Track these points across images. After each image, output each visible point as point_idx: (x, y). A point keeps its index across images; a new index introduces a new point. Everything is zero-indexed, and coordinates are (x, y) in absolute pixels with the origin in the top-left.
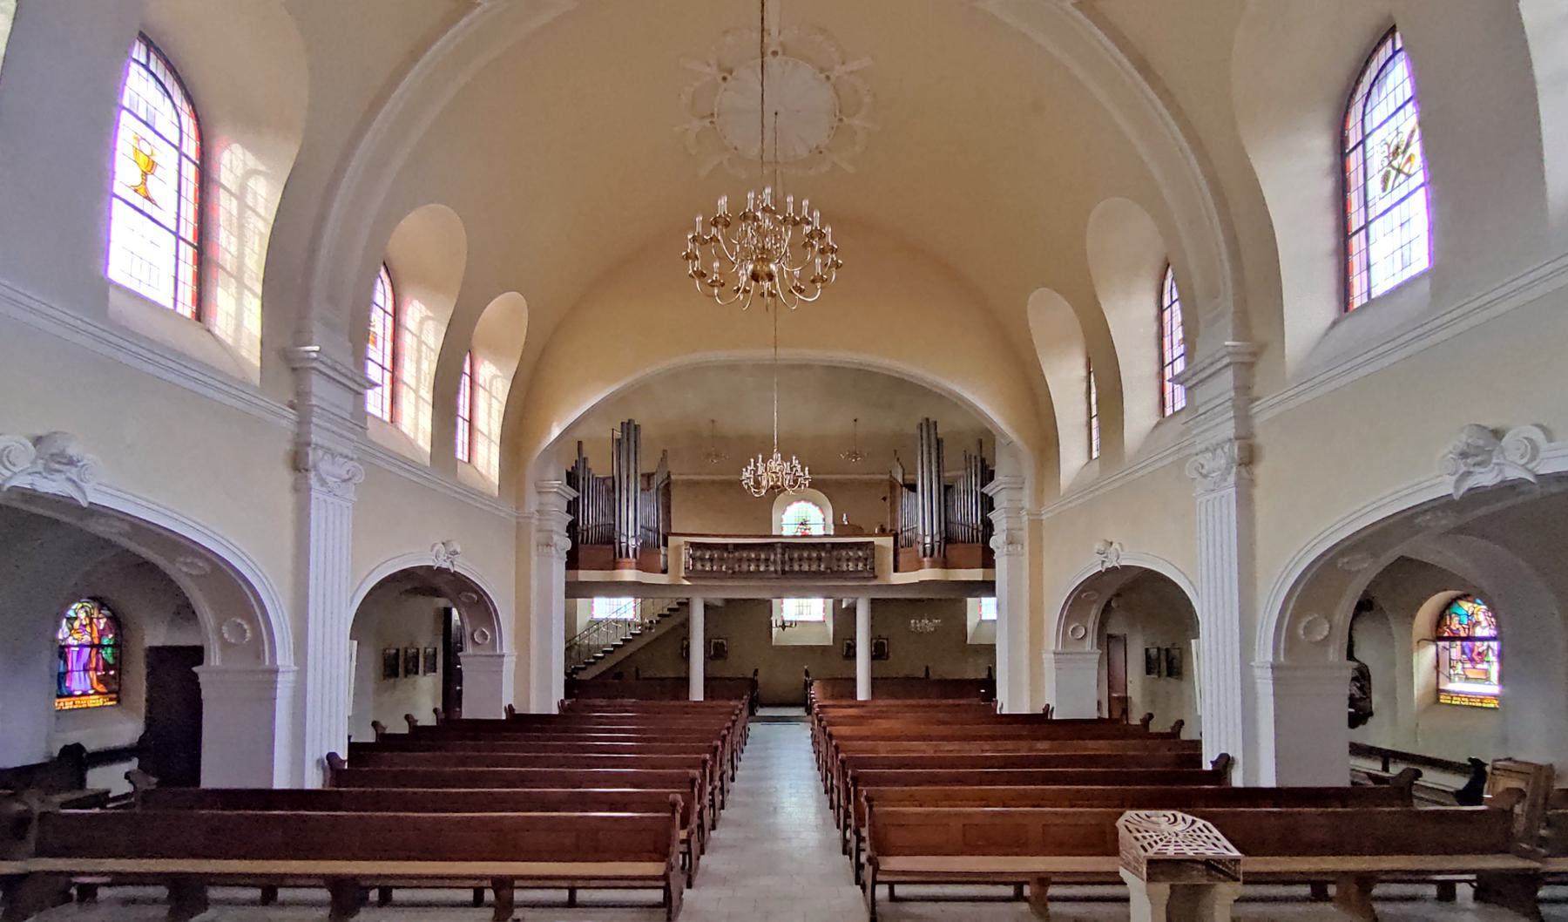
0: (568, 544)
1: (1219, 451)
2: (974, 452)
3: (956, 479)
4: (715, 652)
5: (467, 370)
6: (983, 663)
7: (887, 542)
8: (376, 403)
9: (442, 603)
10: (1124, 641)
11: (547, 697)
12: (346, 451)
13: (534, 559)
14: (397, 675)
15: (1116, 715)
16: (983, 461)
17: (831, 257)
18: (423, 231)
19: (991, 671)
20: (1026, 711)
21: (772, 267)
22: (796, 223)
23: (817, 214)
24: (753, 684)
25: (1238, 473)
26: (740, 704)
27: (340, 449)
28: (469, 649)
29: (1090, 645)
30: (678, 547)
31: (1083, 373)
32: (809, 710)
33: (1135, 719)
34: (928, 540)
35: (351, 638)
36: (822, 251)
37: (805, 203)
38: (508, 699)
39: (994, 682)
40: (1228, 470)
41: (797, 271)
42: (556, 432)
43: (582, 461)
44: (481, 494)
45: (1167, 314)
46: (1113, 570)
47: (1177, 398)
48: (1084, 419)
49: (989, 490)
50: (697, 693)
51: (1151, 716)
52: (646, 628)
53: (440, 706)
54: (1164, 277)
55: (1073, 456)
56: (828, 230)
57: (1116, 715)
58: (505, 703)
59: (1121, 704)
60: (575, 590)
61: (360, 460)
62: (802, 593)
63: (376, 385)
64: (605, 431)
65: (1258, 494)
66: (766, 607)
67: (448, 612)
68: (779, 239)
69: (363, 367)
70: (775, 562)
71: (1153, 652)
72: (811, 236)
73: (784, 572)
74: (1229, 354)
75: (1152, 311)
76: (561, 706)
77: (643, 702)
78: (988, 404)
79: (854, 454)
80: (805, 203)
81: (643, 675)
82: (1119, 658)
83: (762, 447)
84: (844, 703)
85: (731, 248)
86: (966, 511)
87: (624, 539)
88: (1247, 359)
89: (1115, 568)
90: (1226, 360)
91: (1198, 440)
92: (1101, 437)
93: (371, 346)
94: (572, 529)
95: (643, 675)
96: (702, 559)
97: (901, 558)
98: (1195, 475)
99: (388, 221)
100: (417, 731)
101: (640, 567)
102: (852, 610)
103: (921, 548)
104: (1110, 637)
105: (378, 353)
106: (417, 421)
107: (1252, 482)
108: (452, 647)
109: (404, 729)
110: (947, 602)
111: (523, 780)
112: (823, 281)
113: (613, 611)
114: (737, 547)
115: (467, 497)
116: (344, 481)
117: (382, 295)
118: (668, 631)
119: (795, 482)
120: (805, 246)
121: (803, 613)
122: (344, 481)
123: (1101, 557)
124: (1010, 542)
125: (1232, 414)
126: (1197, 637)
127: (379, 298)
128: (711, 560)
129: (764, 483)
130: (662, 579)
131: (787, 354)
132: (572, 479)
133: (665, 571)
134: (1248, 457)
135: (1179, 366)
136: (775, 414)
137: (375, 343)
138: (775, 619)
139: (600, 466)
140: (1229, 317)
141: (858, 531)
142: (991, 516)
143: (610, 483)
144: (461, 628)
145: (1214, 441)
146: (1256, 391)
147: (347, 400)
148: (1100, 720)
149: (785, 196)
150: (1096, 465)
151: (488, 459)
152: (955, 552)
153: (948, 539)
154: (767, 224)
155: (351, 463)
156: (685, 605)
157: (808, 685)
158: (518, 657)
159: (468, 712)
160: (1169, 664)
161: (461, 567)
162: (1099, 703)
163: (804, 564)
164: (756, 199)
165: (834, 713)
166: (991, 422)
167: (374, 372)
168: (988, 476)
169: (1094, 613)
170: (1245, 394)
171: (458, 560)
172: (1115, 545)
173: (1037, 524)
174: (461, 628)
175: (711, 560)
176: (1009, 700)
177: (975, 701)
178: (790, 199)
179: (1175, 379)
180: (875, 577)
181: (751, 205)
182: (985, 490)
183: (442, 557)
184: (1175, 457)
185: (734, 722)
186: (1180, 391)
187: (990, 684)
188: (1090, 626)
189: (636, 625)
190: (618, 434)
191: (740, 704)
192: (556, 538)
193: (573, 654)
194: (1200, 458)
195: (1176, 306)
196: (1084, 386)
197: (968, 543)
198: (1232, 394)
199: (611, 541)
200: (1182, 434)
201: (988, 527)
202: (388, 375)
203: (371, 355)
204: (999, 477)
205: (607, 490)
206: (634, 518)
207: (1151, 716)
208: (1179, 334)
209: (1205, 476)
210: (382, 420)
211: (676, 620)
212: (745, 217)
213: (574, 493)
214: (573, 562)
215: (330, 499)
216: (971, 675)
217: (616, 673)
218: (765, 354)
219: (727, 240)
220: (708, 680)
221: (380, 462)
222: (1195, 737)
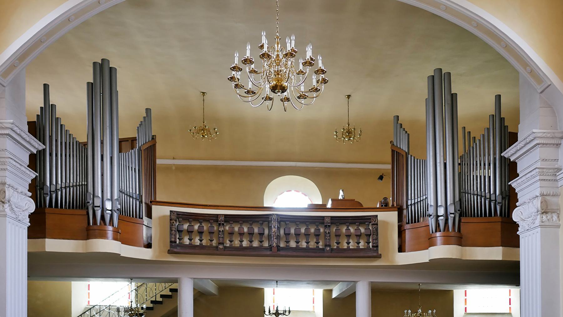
0: (31, 207)
7: (391, 217)
34: (441, 211)
49: (510, 153)
62: (292, 277)
87: (98, 202)
94: (36, 188)
97: (408, 235)
101: (119, 236)
103: (432, 222)
111: (466, 207)
114: (229, 219)
133: (149, 246)
141: (358, 206)
142: (514, 184)
153: (463, 212)
180: (379, 257)
182: (506, 154)
199: (83, 205)
201: (510, 198)
206: (112, 183)
211: (166, 308)
214: (38, 227)
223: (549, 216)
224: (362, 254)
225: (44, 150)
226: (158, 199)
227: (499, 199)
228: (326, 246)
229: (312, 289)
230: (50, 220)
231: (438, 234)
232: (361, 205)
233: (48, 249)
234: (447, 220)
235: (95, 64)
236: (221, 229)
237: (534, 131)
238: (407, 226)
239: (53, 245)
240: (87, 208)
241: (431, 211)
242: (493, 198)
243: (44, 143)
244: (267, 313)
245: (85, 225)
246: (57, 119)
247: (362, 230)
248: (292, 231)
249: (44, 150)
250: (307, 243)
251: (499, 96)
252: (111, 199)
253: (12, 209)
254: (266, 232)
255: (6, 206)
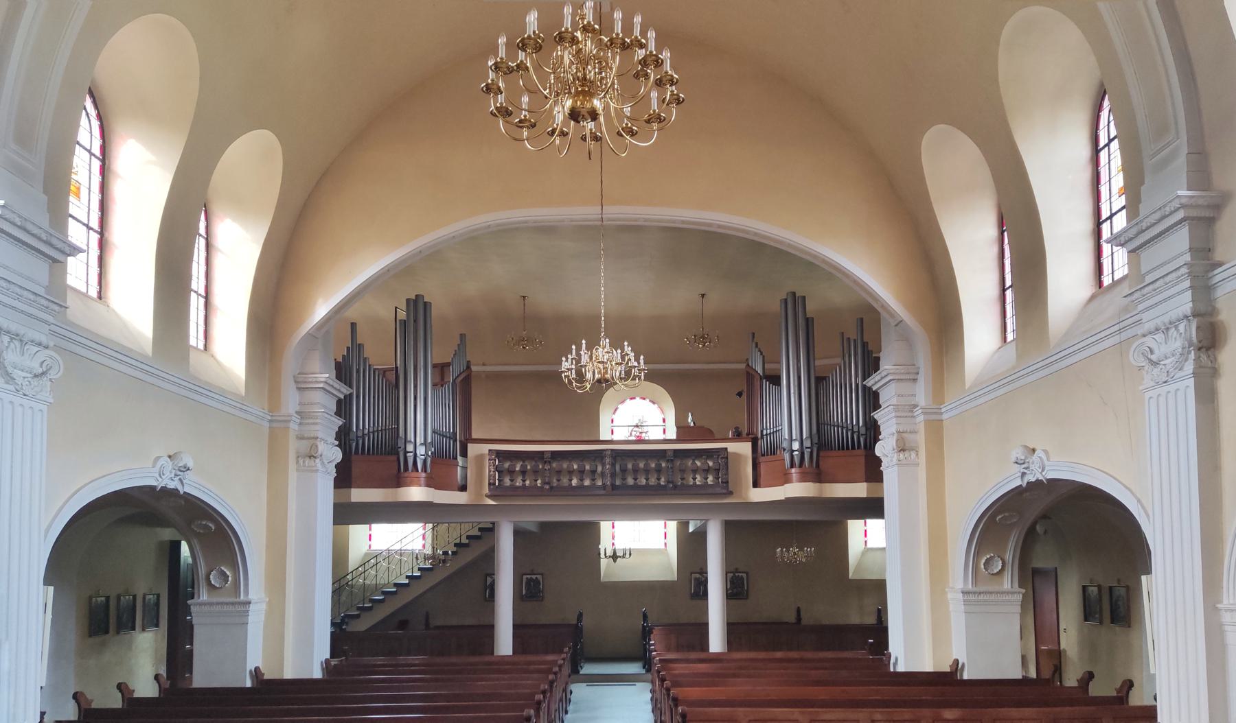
0: (338, 455)
1: (1172, 331)
2: (852, 334)
3: (833, 367)
4: (528, 592)
5: (202, 231)
6: (870, 604)
8: (79, 273)
9: (167, 534)
10: (1052, 576)
11: (305, 653)
12: (38, 337)
13: (293, 476)
14: (107, 632)
15: (1046, 674)
16: (865, 345)
17: (670, 90)
18: (142, 52)
19: (881, 615)
20: (929, 668)
21: (597, 103)
22: (625, 47)
23: (652, 34)
24: (576, 631)
25: (1197, 359)
26: (560, 659)
27: (31, 334)
28: (204, 596)
29: (1008, 582)
30: (480, 458)
31: (991, 231)
32: (648, 665)
33: (1071, 679)
34: (796, 446)
35: (47, 581)
36: (659, 83)
37: (637, 20)
38: (255, 658)
39: (885, 630)
40: (1184, 356)
41: (627, 110)
42: (321, 310)
43: (356, 348)
44: (223, 393)
45: (1103, 155)
46: (1053, 482)
47: (1117, 262)
48: (994, 291)
49: (873, 382)
50: (505, 644)
51: (1090, 676)
52: (437, 561)
53: (163, 671)
54: (1099, 108)
55: (982, 336)
56: (666, 55)
57: (1046, 674)
58: (251, 666)
59: (1052, 659)
60: (346, 514)
61: (57, 348)
63: (81, 251)
64: (385, 310)
65: (1225, 387)
66: (590, 532)
67: (176, 546)
68: (603, 65)
69: (63, 228)
70: (603, 475)
71: (1093, 590)
72: (644, 62)
73: (614, 487)
74: (1183, 206)
75: (1085, 151)
76: (326, 666)
77: (439, 660)
78: (866, 267)
79: (704, 338)
80: (637, 20)
81: (435, 622)
82: (1049, 599)
83: (583, 329)
84: (693, 655)
85: (544, 78)
86: (845, 410)
87: (410, 448)
88: (1207, 213)
89: (1039, 482)
90: (1180, 215)
91: (1145, 316)
92: (1017, 314)
93: (72, 199)
94: (343, 437)
95: (435, 622)
96: (511, 472)
97: (763, 468)
98: (1142, 362)
99: (98, 31)
100: (134, 705)
101: (432, 483)
102: (701, 535)
103: (787, 457)
104: (1036, 572)
105: (82, 206)
106: (132, 304)
107: (1215, 372)
108: (180, 589)
109: (116, 702)
110: (823, 526)
112: (660, 120)
113: (402, 540)
115: (200, 396)
116: (35, 376)
117: (87, 132)
118: (462, 568)
119: (628, 373)
120: (637, 76)
121: (640, 542)
122: (35, 376)
123: (1020, 469)
124: (902, 448)
125: (1187, 283)
126: (1148, 571)
127: (83, 136)
128: (523, 472)
129: (589, 376)
130: (459, 498)
131: (617, 212)
132: (343, 371)
133: (463, 488)
134: (1209, 338)
135: (1120, 222)
136: (603, 288)
137: (78, 195)
138: (605, 545)
139: (380, 353)
140: (1181, 162)
141: (708, 435)
142: (877, 415)
143: (392, 376)
144: (194, 567)
145: (1166, 319)
146: (1218, 256)
147: (40, 270)
148: (1025, 681)
149: (612, 10)
150: (1011, 350)
151: (227, 346)
152: (831, 461)
154: (589, 46)
155: (47, 352)
156: (489, 531)
157: (646, 633)
158: (269, 603)
159: (202, 677)
160: (1115, 608)
161: (193, 486)
162: (1024, 658)
163: (640, 478)
164: (574, 15)
165: (680, 669)
166: (876, 298)
167: (76, 234)
168: (871, 364)
169: (1010, 553)
170: (1204, 261)
171: (189, 477)
172: (1039, 453)
173: (935, 428)
174: (194, 567)
175: (523, 472)
176: (910, 651)
177: (861, 654)
178: (618, 15)
179: (1116, 240)
180: (731, 493)
181: (567, 23)
183: (168, 474)
184: (1116, 339)
185: (552, 683)
186: (1121, 255)
187: (879, 632)
188: (1009, 556)
189: (426, 558)
190: (402, 315)
191: (560, 659)
192: (322, 447)
193: (343, 598)
194: (1149, 341)
195: (1115, 145)
196: (995, 250)
197: (848, 449)
198: (1187, 257)
200: (1126, 309)
201: (873, 431)
202: (95, 237)
203: (72, 210)
204: (886, 366)
205: (389, 383)
206: (421, 424)
207: (1090, 676)
208: (1119, 181)
209: (1154, 364)
210: (86, 295)
212: (561, 39)
213: (346, 390)
214: (344, 478)
215: (18, 400)
216: (855, 619)
217: (401, 621)
218: (587, 212)
219: (538, 68)
220: (519, 629)
221: (83, 354)
222: (1148, 702)
223: (907, 454)
224: (710, 491)
225: (351, 395)
226: (474, 436)
227: (863, 431)
228: (668, 482)
229: (662, 522)
230: (356, 470)
231: (793, 470)
232: (711, 432)
233: (353, 500)
234: (802, 454)
235: (408, 300)
236: (547, 467)
237: (1180, 193)
238: (762, 459)
239: (359, 495)
240: (398, 454)
241: (785, 445)
242: (856, 429)
243: (351, 387)
244: (602, 555)
245: (396, 471)
246: (365, 359)
247: (711, 464)
248: (630, 466)
249: (351, 395)
250: (647, 479)
251: (862, 319)
252: (425, 444)
253: (323, 463)
254: (600, 469)
255: (318, 461)
